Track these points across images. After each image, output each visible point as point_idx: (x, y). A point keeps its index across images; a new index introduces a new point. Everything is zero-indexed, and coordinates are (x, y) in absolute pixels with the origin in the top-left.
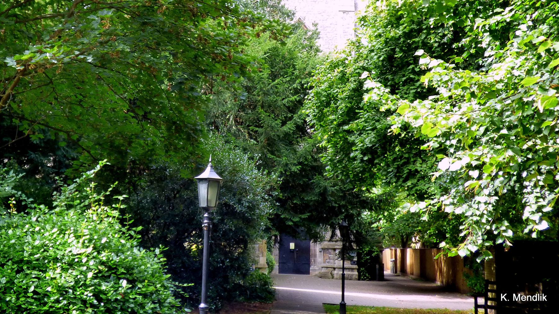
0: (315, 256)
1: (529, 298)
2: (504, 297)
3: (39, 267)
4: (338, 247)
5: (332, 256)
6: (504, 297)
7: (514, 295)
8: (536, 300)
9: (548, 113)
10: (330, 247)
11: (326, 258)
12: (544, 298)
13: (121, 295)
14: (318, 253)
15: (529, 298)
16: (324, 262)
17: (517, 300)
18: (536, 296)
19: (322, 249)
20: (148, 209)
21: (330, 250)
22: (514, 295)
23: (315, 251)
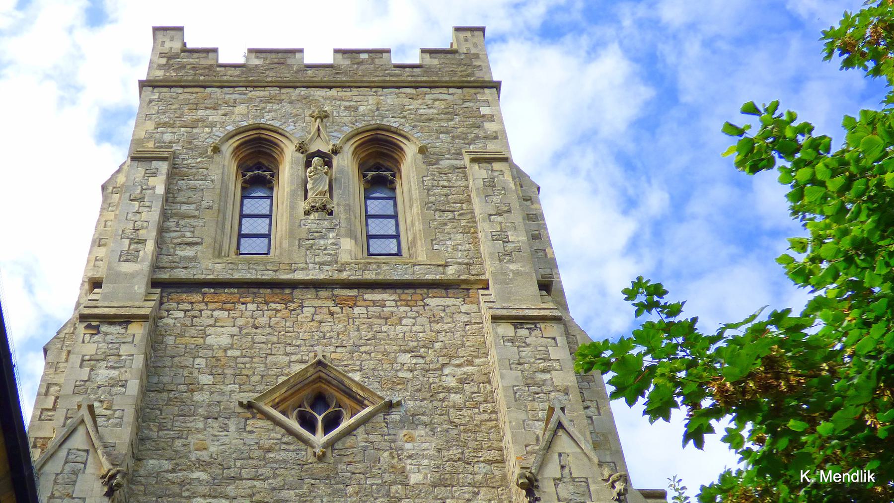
17: (826, 480)
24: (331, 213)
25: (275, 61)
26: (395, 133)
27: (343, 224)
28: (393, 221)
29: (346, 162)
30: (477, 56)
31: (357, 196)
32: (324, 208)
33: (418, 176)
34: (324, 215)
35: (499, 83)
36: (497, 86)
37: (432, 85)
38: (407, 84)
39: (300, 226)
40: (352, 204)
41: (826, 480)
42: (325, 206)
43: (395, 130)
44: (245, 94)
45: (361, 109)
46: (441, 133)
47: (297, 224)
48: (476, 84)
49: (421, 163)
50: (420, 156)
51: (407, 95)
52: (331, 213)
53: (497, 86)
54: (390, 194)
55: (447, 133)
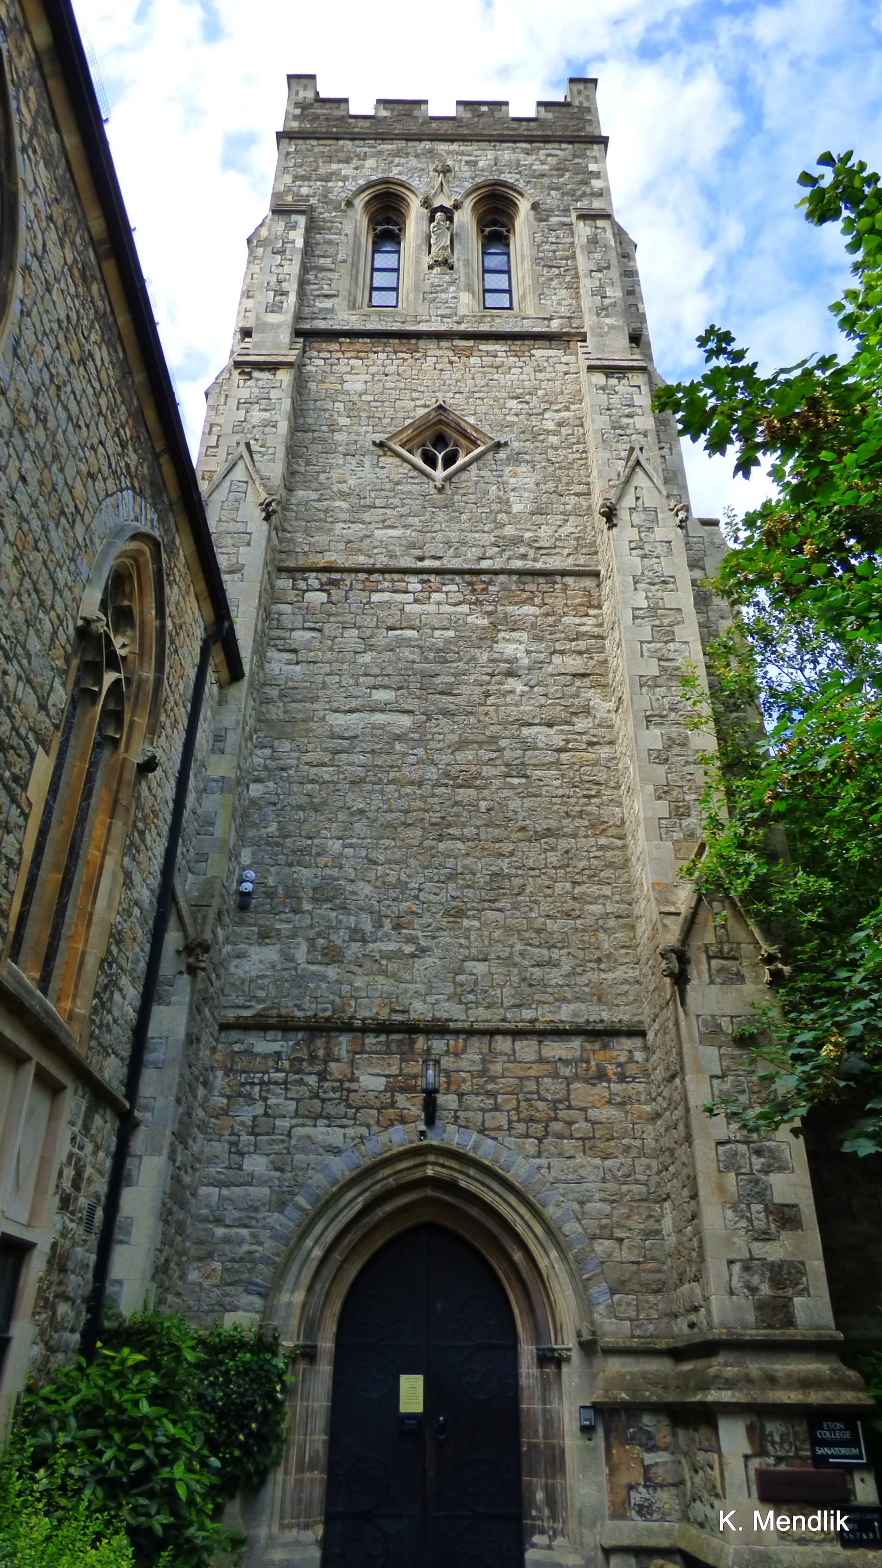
0: (556, 1462)
1: (799, 1521)
2: (727, 1519)
3: (519, 932)
4: (727, 1396)
5: (662, 1457)
6: (727, 1519)
7: (757, 1514)
8: (795, 1518)
9: (160, 1276)
10: (649, 1395)
11: (625, 1478)
12: (841, 1522)
13: (54, 1439)
14: (571, 1441)
15: (799, 1521)
16: (619, 1513)
17: (764, 1528)
18: (818, 1518)
19: (596, 1408)
20: (832, 463)
21: (647, 1420)
22: (757, 1514)
23: (550, 1422)
34: (446, 268)
45: (481, 164)
50: (532, 213)
51: (523, 149)
52: (452, 268)
55: (557, 189)
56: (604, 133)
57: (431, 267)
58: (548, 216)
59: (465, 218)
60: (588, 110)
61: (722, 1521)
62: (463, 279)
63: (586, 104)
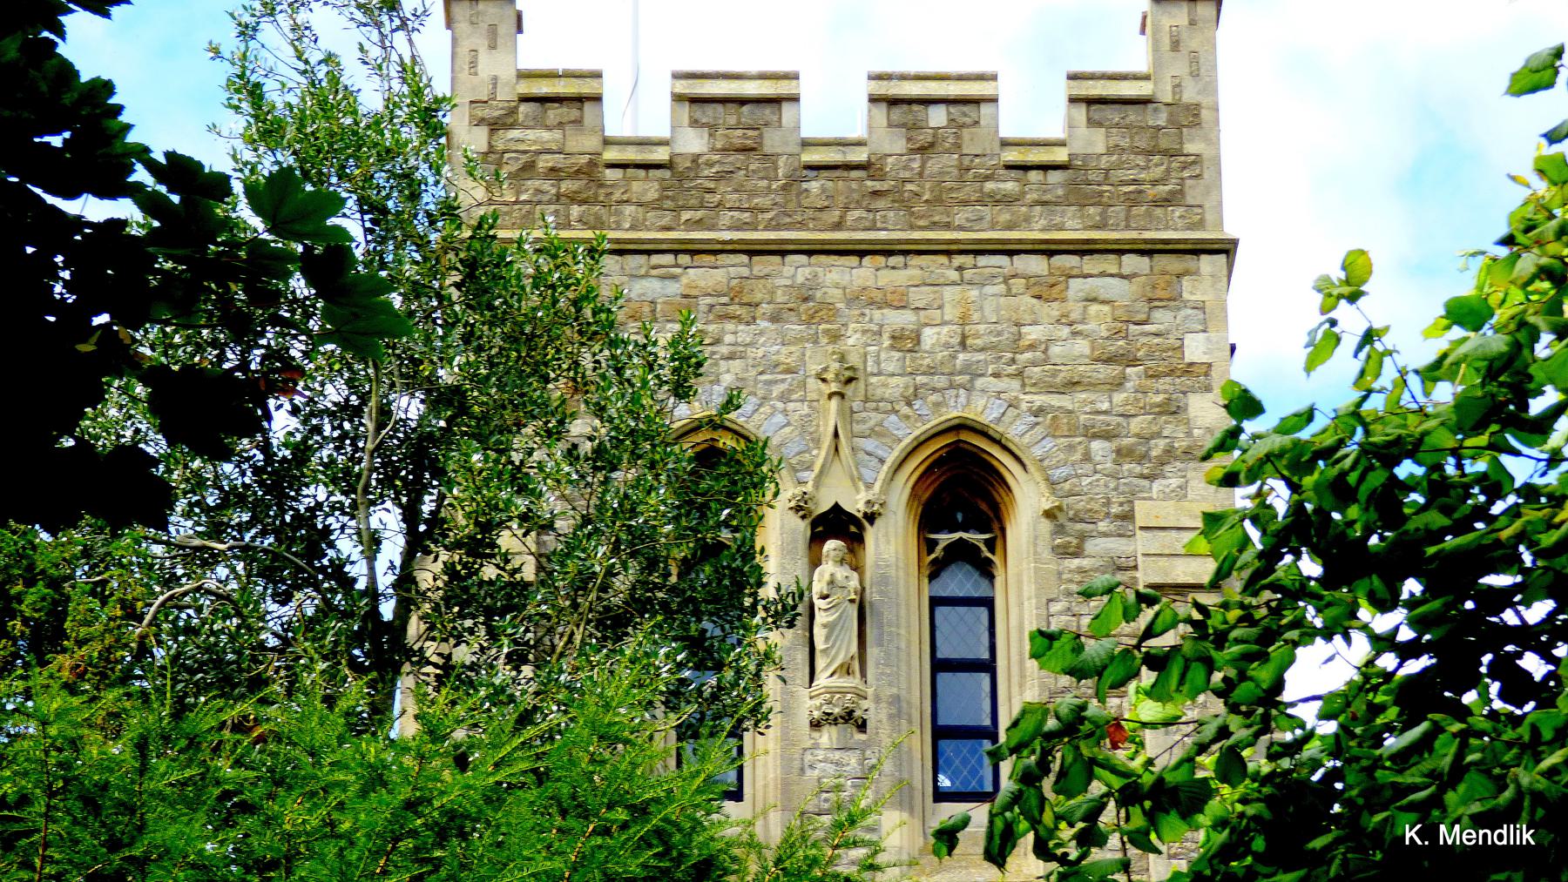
1: (1485, 835)
2: (1413, 833)
8: (1481, 832)
12: (1526, 836)
15: (1485, 835)
17: (1450, 842)
18: (1504, 832)
24: (862, 726)
25: (738, 142)
26: (998, 442)
27: (888, 767)
28: (983, 612)
29: (892, 548)
30: (1194, 111)
31: (915, 662)
32: (848, 716)
33: (1037, 596)
34: (851, 729)
35: (1234, 243)
36: (1226, 249)
37: (1086, 247)
38: (1029, 247)
39: (802, 769)
40: (903, 693)
41: (1450, 842)
42: (850, 713)
43: (997, 436)
44: (674, 277)
45: (929, 336)
46: (1095, 436)
47: (797, 764)
48: (1182, 247)
49: (1046, 554)
50: (1046, 526)
51: (1031, 280)
52: (862, 726)
53: (1226, 249)
54: (981, 591)
55: (1107, 436)
56: (1230, 230)
57: (816, 725)
58: (1083, 537)
59: (892, 545)
60: (1194, 111)
61: (1408, 836)
62: (888, 767)
63: (1189, 96)
